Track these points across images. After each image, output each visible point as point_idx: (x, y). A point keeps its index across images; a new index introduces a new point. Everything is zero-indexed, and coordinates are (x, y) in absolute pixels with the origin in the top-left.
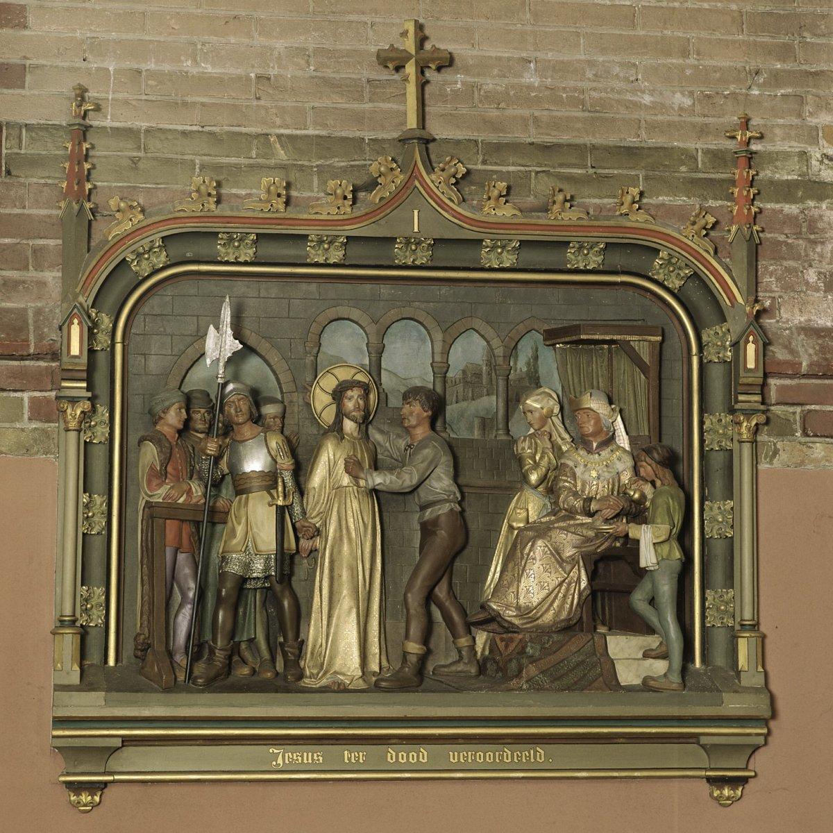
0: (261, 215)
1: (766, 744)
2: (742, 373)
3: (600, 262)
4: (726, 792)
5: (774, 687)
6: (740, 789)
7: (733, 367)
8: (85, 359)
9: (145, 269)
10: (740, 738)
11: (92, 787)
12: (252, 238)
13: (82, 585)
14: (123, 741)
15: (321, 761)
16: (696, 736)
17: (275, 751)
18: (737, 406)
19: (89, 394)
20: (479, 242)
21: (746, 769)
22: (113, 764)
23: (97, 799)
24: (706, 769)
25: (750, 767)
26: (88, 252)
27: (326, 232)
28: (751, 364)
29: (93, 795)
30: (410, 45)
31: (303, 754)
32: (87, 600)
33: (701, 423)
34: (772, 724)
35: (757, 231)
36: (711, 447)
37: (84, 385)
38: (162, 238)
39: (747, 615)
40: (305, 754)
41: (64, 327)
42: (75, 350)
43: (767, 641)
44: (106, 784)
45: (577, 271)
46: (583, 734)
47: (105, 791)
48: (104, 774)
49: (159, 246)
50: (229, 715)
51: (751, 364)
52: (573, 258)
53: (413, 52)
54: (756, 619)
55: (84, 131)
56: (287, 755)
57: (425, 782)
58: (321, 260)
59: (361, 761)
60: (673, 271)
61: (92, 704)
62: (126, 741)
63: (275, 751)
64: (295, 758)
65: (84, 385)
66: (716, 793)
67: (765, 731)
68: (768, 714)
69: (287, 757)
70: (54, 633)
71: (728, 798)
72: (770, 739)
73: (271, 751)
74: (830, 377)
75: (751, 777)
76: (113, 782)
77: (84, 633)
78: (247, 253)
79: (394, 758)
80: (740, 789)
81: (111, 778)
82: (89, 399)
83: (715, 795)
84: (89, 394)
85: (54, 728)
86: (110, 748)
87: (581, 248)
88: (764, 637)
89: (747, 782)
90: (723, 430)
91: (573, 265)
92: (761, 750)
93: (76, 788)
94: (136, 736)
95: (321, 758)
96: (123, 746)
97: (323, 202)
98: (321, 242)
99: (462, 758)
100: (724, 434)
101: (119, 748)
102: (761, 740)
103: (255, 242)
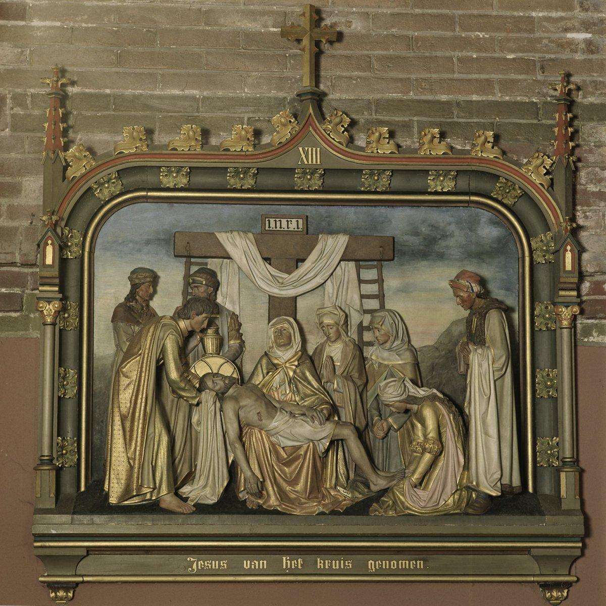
0: (236, 153)
1: (583, 554)
2: (562, 274)
3: (320, 184)
4: (61, 593)
5: (589, 510)
6: (566, 591)
7: (556, 266)
8: (55, 272)
9: (106, 194)
10: (551, 550)
11: (558, 586)
12: (320, 172)
13: (58, 436)
14: (88, 551)
15: (226, 567)
16: (527, 550)
17: (192, 559)
18: (556, 300)
19: (60, 296)
20: (426, 172)
21: (569, 574)
22: (82, 567)
23: (70, 595)
24: (534, 575)
25: (573, 572)
26: (63, 180)
27: (240, 164)
28: (569, 267)
29: (562, 591)
30: (305, 23)
31: (332, 561)
32: (62, 447)
33: (532, 309)
34: (587, 541)
35: (573, 161)
36: (540, 327)
37: (57, 289)
38: (118, 171)
39: (568, 453)
40: (334, 562)
41: (40, 247)
42: (49, 261)
43: (586, 476)
44: (77, 584)
45: (436, 193)
46: (439, 547)
47: (570, 589)
48: (76, 575)
49: (115, 178)
50: (273, 533)
51: (569, 267)
52: (366, 181)
53: (308, 28)
54: (575, 457)
55: (62, 98)
56: (199, 562)
57: (168, 584)
58: (171, 185)
59: (300, 567)
60: (508, 192)
61: (61, 523)
62: (89, 550)
63: (192, 559)
64: (206, 565)
65: (57, 289)
66: (548, 595)
67: (580, 545)
68: (581, 530)
69: (199, 565)
70: (35, 469)
71: (557, 599)
72: (587, 551)
73: (188, 559)
74: (603, 273)
75: (573, 582)
76: (83, 582)
77: (59, 471)
78: (316, 183)
79: (217, 566)
80: (566, 591)
81: (80, 579)
82: (61, 300)
83: (547, 596)
84: (60, 296)
85: (35, 541)
86: (78, 556)
87: (305, 173)
88: (582, 471)
89: (571, 586)
90: (549, 315)
91: (366, 188)
92: (579, 562)
93: (546, 586)
94: (519, 547)
95: (350, 565)
96: (88, 555)
97: (182, 140)
98: (372, 174)
99: (293, 565)
100: (550, 318)
101: (85, 557)
102: (578, 552)
103: (322, 176)
